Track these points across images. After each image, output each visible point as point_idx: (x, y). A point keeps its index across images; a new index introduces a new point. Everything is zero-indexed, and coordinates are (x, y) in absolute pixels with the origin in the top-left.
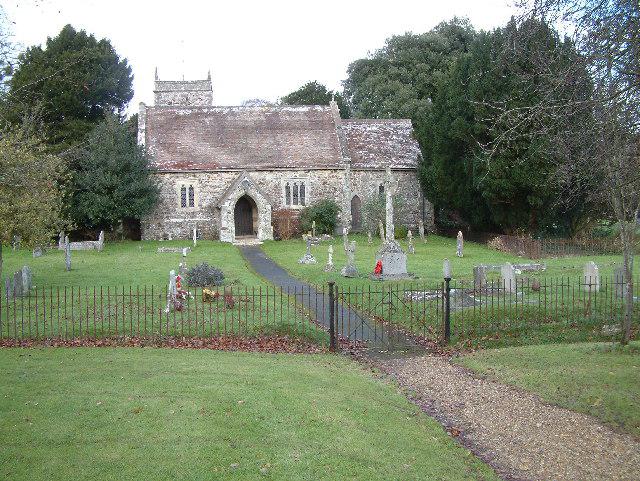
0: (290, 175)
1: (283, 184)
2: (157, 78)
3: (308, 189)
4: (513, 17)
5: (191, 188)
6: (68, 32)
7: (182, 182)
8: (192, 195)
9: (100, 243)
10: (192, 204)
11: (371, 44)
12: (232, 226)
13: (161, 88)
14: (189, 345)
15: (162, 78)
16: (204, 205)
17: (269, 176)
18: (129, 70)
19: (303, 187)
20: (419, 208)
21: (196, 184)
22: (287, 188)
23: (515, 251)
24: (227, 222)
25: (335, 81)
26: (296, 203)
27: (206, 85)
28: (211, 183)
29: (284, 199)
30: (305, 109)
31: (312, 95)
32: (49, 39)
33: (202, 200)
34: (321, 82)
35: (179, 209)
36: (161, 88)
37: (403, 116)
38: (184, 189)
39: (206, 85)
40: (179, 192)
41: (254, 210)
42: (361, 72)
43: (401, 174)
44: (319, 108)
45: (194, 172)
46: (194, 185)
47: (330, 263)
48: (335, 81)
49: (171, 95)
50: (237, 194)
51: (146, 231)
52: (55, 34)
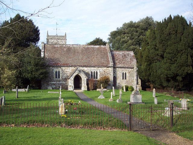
0: (92, 68)
2: (48, 34)
4: (170, 16)
5: (59, 72)
6: (18, 17)
8: (59, 74)
9: (27, 90)
10: (59, 77)
11: (117, 25)
12: (73, 85)
13: (49, 38)
14: (179, 131)
18: (39, 31)
19: (97, 72)
21: (60, 70)
23: (173, 96)
25: (105, 38)
27: (64, 37)
30: (98, 46)
31: (98, 42)
32: (11, 19)
33: (62, 76)
34: (101, 38)
35: (55, 79)
36: (49, 38)
37: (130, 50)
38: (56, 72)
39: (64, 37)
40: (55, 73)
41: (80, 80)
42: (114, 35)
44: (102, 46)
48: (105, 38)
49: (53, 40)
51: (43, 86)
52: (13, 16)
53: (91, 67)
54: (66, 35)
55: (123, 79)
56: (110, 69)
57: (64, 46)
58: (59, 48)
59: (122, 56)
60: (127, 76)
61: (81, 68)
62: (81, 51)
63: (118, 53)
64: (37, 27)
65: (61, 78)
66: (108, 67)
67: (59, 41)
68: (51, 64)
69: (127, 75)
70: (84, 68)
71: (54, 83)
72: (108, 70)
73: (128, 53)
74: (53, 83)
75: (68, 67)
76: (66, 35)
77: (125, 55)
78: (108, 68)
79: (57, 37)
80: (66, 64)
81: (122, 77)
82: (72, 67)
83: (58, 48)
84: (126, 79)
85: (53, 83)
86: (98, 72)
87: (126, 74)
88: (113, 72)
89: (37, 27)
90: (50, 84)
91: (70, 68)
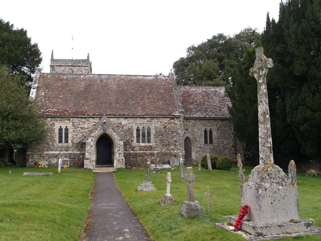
0: (139, 121)
1: (135, 128)
2: (52, 56)
3: (153, 132)
5: (67, 129)
7: (58, 125)
8: (67, 134)
10: (67, 141)
12: (94, 158)
13: (55, 63)
15: (55, 58)
16: (75, 142)
17: (124, 122)
20: (233, 146)
21: (70, 126)
22: (138, 130)
24: (91, 153)
26: (144, 142)
27: (87, 63)
28: (80, 126)
29: (135, 139)
33: (73, 138)
36: (55, 63)
38: (61, 129)
39: (87, 63)
40: (57, 131)
42: (180, 66)
43: (220, 123)
45: (69, 118)
46: (69, 127)
47: (169, 195)
50: (98, 133)
53: (136, 117)
54: (88, 57)
55: (206, 142)
56: (177, 121)
57: (82, 77)
58: (70, 81)
59: (201, 97)
60: (214, 137)
61: (115, 119)
62: (115, 87)
63: (193, 89)
64: (8, 23)
65: (70, 141)
66: (173, 119)
67: (75, 69)
68: (48, 112)
69: (214, 134)
70: (122, 119)
71: (54, 154)
72: (172, 125)
73: (212, 89)
74: (53, 152)
75: (85, 118)
76: (88, 57)
77: (207, 94)
78: (172, 121)
79: (75, 63)
80: (82, 112)
81: (203, 139)
82: (94, 118)
83: (68, 80)
84: (211, 142)
85: (53, 152)
86: (152, 127)
87: (211, 132)
88: (183, 128)
89: (35, 46)
90: (47, 155)
91: (91, 119)
